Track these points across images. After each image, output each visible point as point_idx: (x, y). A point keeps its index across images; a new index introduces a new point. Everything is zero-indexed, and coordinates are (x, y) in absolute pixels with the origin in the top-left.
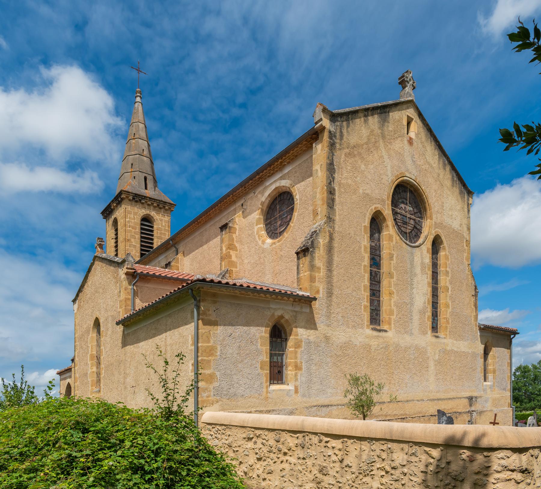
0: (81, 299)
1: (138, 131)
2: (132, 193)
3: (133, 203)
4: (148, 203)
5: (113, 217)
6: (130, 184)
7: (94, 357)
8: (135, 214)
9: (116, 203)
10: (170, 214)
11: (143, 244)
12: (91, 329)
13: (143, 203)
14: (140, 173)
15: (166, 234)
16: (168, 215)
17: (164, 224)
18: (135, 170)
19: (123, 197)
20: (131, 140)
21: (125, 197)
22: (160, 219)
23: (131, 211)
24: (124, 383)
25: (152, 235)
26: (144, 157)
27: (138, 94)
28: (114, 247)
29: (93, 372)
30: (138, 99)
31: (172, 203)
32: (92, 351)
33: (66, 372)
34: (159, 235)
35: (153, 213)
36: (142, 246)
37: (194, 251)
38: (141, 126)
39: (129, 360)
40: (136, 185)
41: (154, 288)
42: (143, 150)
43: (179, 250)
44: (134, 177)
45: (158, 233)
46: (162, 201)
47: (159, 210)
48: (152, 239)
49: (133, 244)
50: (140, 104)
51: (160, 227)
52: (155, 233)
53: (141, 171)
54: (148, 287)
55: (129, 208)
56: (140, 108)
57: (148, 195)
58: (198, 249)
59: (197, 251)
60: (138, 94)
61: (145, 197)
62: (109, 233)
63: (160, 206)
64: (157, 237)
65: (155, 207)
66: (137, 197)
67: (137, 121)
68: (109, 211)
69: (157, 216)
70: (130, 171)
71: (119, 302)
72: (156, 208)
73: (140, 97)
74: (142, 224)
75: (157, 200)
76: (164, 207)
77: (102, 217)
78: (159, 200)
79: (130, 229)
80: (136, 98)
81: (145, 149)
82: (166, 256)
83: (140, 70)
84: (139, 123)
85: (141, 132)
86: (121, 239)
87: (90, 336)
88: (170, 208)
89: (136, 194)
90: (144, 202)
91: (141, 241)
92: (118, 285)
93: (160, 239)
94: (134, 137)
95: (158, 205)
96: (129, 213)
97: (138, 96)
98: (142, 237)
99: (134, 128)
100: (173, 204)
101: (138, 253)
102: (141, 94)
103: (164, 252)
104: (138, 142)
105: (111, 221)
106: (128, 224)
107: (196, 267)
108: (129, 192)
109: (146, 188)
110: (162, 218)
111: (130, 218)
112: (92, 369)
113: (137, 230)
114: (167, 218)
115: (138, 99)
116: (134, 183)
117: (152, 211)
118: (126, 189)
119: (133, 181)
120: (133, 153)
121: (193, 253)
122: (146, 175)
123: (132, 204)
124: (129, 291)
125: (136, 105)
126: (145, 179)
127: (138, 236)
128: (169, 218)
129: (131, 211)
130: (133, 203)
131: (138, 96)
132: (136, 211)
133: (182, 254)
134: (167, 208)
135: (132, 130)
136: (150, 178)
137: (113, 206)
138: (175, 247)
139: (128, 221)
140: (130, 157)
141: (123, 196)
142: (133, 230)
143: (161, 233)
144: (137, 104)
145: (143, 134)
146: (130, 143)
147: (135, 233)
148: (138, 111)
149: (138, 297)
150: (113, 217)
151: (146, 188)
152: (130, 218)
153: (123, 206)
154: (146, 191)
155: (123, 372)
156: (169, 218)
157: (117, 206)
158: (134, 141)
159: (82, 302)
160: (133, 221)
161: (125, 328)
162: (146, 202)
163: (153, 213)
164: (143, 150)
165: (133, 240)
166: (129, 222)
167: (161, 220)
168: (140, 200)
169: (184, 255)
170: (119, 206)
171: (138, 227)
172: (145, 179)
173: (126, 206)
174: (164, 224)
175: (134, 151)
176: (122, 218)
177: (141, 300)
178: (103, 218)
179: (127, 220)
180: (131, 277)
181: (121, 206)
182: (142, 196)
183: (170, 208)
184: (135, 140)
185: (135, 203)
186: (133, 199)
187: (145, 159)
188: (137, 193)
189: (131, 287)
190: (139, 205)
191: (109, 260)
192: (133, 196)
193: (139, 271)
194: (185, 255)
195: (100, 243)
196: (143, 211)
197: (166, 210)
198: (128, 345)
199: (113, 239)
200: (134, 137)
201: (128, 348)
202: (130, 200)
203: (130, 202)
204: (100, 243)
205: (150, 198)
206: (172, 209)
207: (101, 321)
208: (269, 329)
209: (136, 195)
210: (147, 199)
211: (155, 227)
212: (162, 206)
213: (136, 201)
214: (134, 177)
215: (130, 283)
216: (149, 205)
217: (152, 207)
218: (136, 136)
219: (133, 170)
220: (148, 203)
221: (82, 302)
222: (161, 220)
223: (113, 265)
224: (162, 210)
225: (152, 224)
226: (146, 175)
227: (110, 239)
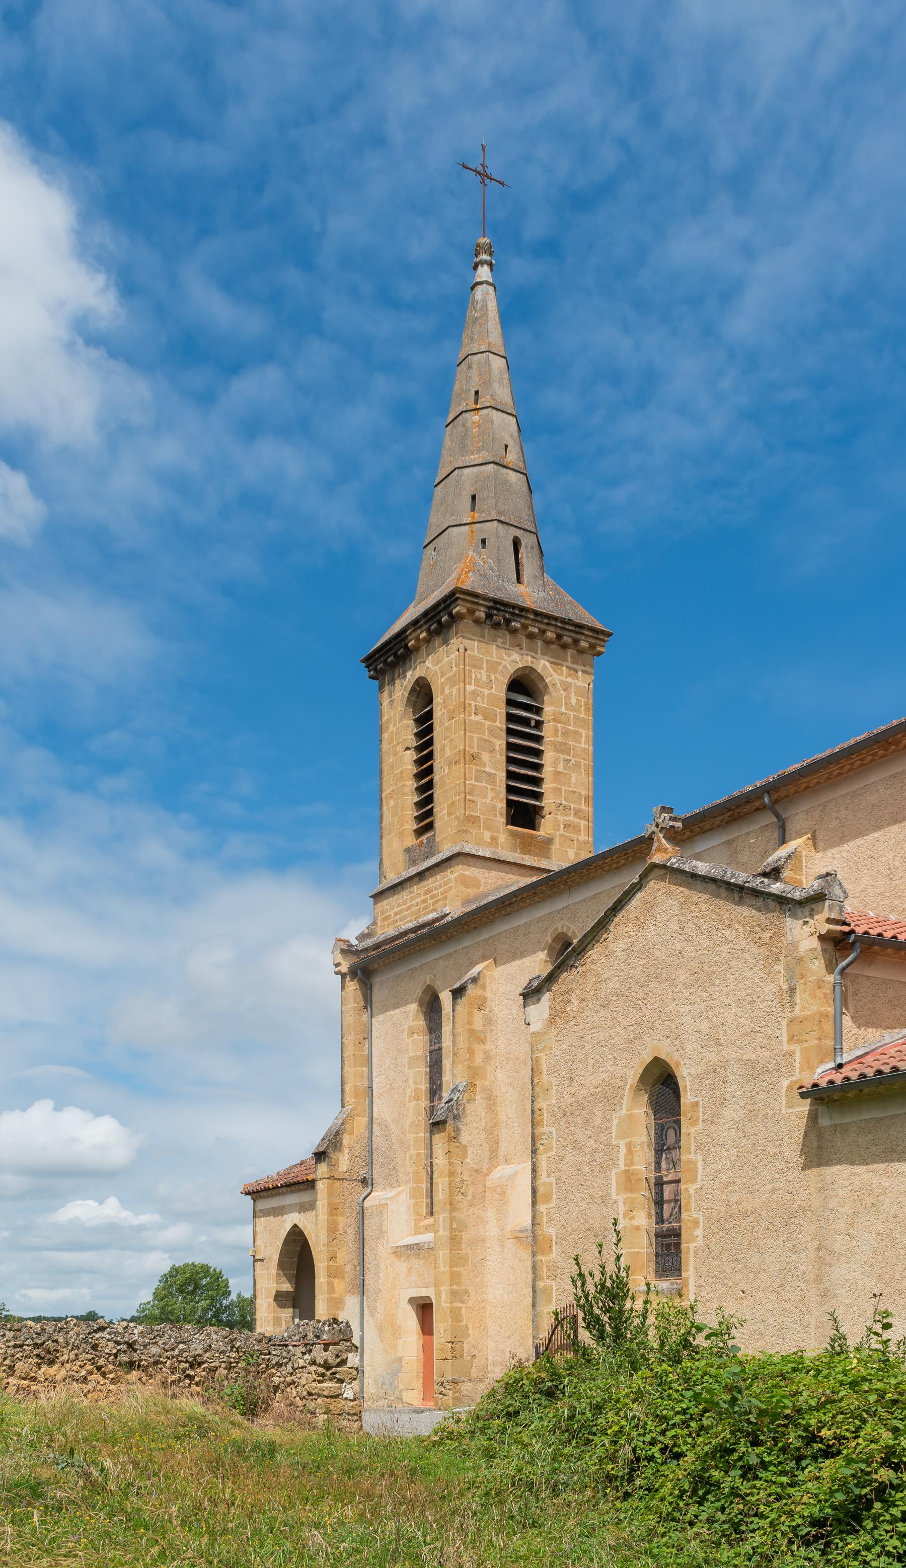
0: (568, 992)
1: (488, 383)
2: (485, 598)
3: (486, 631)
4: (530, 629)
5: (411, 676)
6: (473, 567)
7: (639, 1180)
8: (493, 667)
9: (428, 631)
10: (592, 666)
11: (513, 768)
12: (627, 1094)
13: (514, 632)
14: (500, 525)
15: (580, 735)
16: (588, 669)
17: (574, 702)
18: (484, 517)
19: (458, 613)
20: (467, 415)
21: (464, 611)
22: (562, 683)
23: (481, 659)
24: (819, 1279)
25: (538, 739)
26: (510, 472)
27: (485, 257)
28: (411, 776)
29: (638, 1228)
30: (484, 273)
31: (600, 626)
32: (630, 1162)
33: (284, 1190)
34: (559, 739)
35: (543, 665)
36: (510, 775)
37: (859, 834)
38: (498, 364)
39: (847, 1209)
40: (491, 568)
41: (884, 981)
42: (506, 446)
43: (791, 827)
44: (484, 541)
45: (556, 730)
46: (570, 622)
47: (561, 651)
48: (538, 753)
49: (487, 769)
50: (491, 289)
51: (563, 710)
52: (547, 731)
53: (503, 519)
54: (869, 978)
55: (475, 647)
56: (492, 305)
57: (528, 604)
58: (878, 827)
59: (876, 835)
60: (485, 257)
61: (522, 609)
62: (391, 728)
63: (565, 639)
64: (554, 744)
65: (548, 642)
66: (498, 610)
67: (482, 349)
68: (395, 655)
69: (555, 674)
70: (469, 520)
71: (785, 1022)
72: (553, 647)
73: (490, 265)
74: (510, 703)
75: (556, 619)
76: (576, 642)
77: (366, 673)
78: (563, 621)
79: (479, 718)
80: (475, 267)
81: (510, 443)
82: (729, 843)
83: (488, 172)
84: (491, 356)
85: (496, 386)
86: (448, 753)
87: (623, 1112)
88: (593, 646)
89: (496, 601)
90: (518, 625)
91: (510, 760)
92: (780, 967)
93: (563, 752)
94: (476, 402)
95: (559, 637)
96: (475, 666)
97: (482, 263)
98: (510, 747)
99: (474, 373)
100: (603, 632)
101: (501, 801)
102: (491, 254)
103: (719, 826)
104: (491, 421)
105: (402, 687)
106: (473, 704)
107: (870, 889)
108: (476, 595)
109: (519, 580)
110: (569, 680)
111: (477, 682)
112: (632, 1218)
113: (498, 724)
114: (582, 681)
115: (484, 273)
116: (484, 559)
117: (539, 655)
118: (467, 586)
119: (480, 555)
120: (475, 458)
121: (860, 841)
122: (518, 533)
123: (483, 636)
124: (828, 989)
125: (479, 292)
126: (516, 543)
127: (500, 743)
128: (590, 678)
129: (481, 659)
130: (487, 631)
131: (482, 263)
132: (495, 659)
133: (810, 842)
134: (584, 644)
135: (468, 379)
136: (527, 541)
137: (417, 639)
138: (777, 815)
139: (473, 693)
140: (466, 471)
141: (459, 609)
142: (487, 723)
143: (566, 733)
144: (479, 291)
145: (503, 393)
146: (464, 425)
147: (491, 732)
148: (485, 314)
149: (847, 1009)
150: (409, 674)
151: (519, 580)
152: (477, 682)
153: (456, 642)
154: (521, 588)
155: (813, 1245)
156: (590, 678)
157: (428, 641)
158: (476, 418)
159: (575, 1001)
160: (486, 692)
161: (821, 1109)
162: (525, 627)
163: (543, 665)
164: (506, 446)
165: (485, 756)
166: (475, 694)
167: (567, 688)
168: (508, 622)
169: (815, 846)
170: (437, 641)
171: (501, 711)
172: (516, 543)
173: (467, 643)
174: (574, 702)
175: (478, 452)
176: (452, 682)
177: (855, 1020)
178: (371, 677)
179: (470, 688)
180: (830, 947)
181: (446, 642)
182: (514, 607)
183: (593, 646)
184: (481, 412)
185: (493, 632)
186: (489, 616)
187: (513, 476)
188: (499, 595)
189: (831, 978)
190: (505, 637)
191: (735, 885)
192: (489, 608)
193: (860, 930)
194: (821, 845)
195: (671, 823)
196: (515, 656)
197: (581, 652)
198: (840, 1162)
199: (408, 749)
200: (476, 402)
201: (839, 1173)
202: (477, 622)
203: (476, 629)
204: (671, 823)
205: (537, 613)
206: (599, 649)
207: (685, 1075)
208: (413, 1007)
209: (498, 605)
210: (527, 618)
211: (548, 709)
212: (570, 640)
213: (496, 626)
214: (484, 541)
215: (830, 968)
216: (531, 636)
217: (540, 643)
218: (484, 401)
219: (477, 517)
220: (530, 629)
221: (575, 1001)
222: (567, 688)
223: (799, 911)
224: (570, 652)
225: (535, 700)
226: (518, 533)
227: (399, 749)
